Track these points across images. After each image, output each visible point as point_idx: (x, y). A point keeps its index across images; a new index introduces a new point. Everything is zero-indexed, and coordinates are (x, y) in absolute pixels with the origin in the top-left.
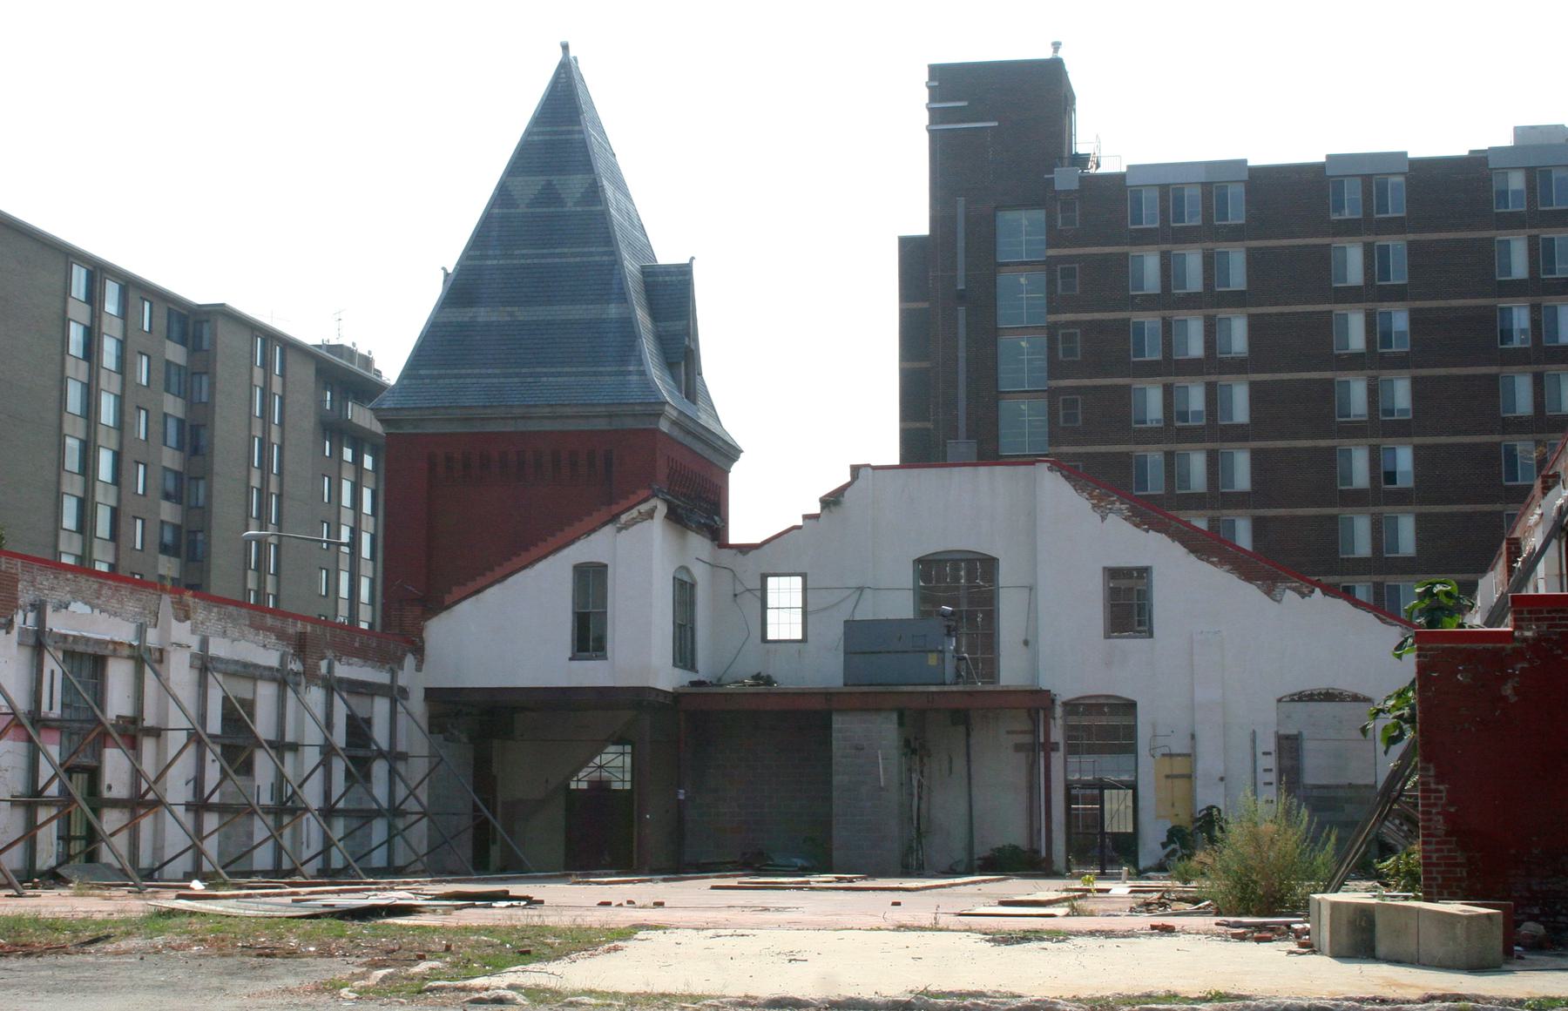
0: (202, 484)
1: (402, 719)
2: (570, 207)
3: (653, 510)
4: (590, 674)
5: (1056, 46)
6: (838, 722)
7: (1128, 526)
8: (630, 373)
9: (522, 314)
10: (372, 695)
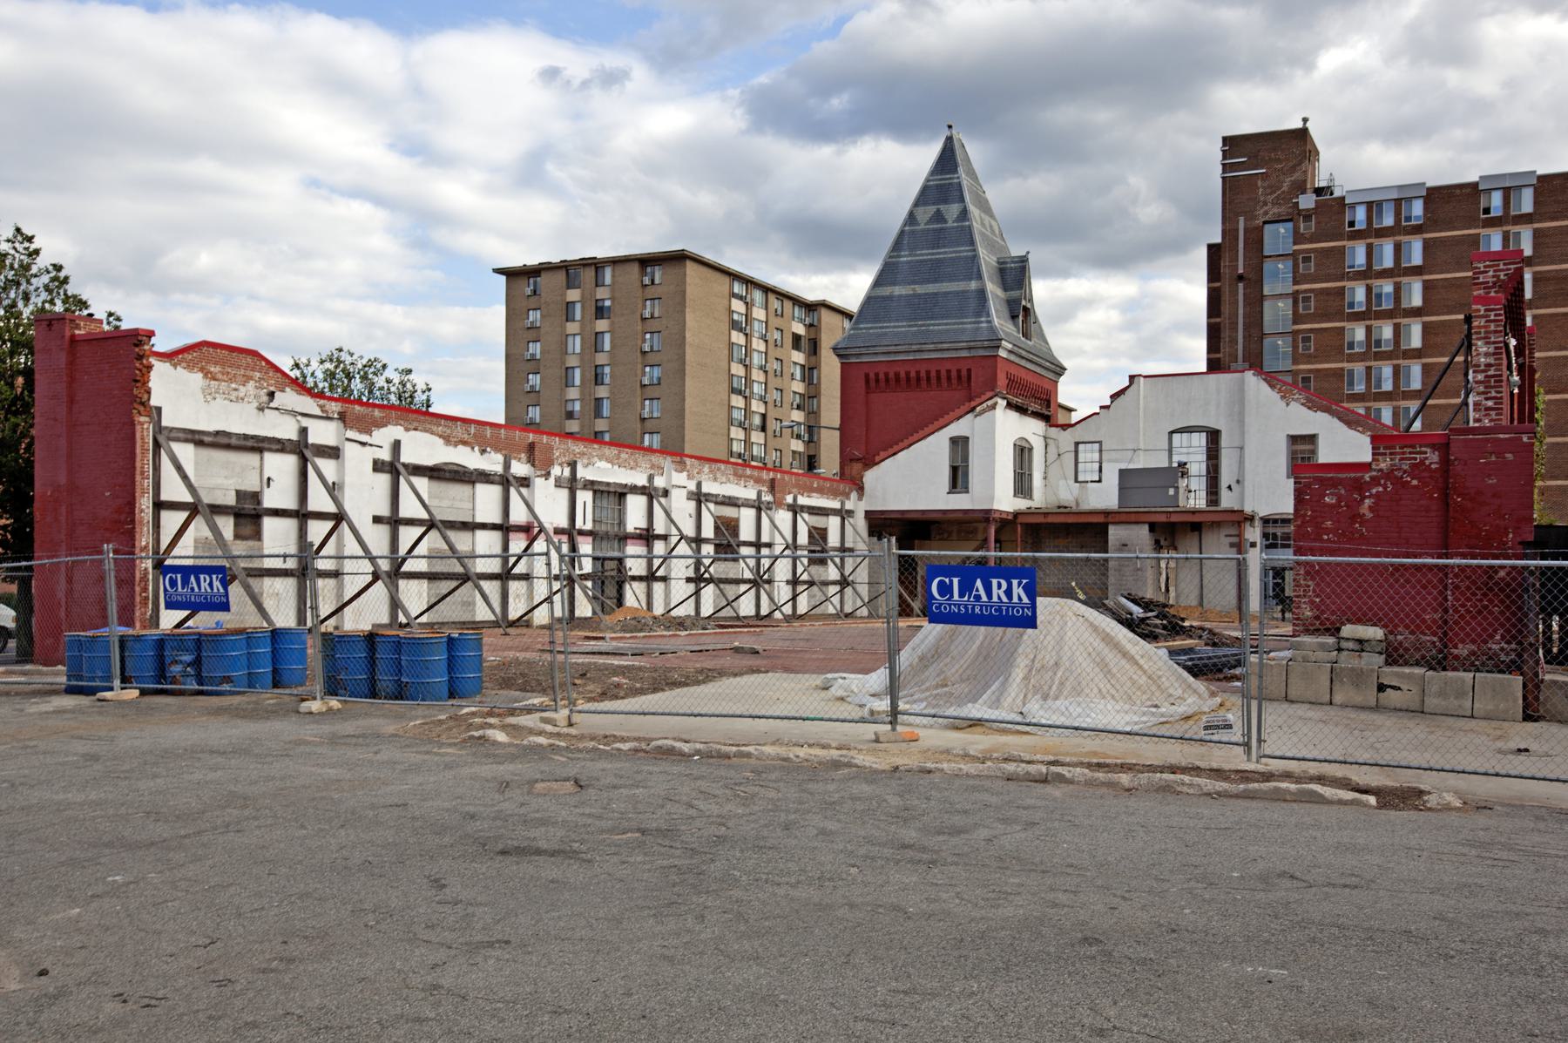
0: (815, 400)
1: (848, 528)
2: (950, 224)
3: (996, 404)
4: (959, 502)
5: (1305, 120)
7: (1304, 409)
8: (982, 322)
10: (828, 515)
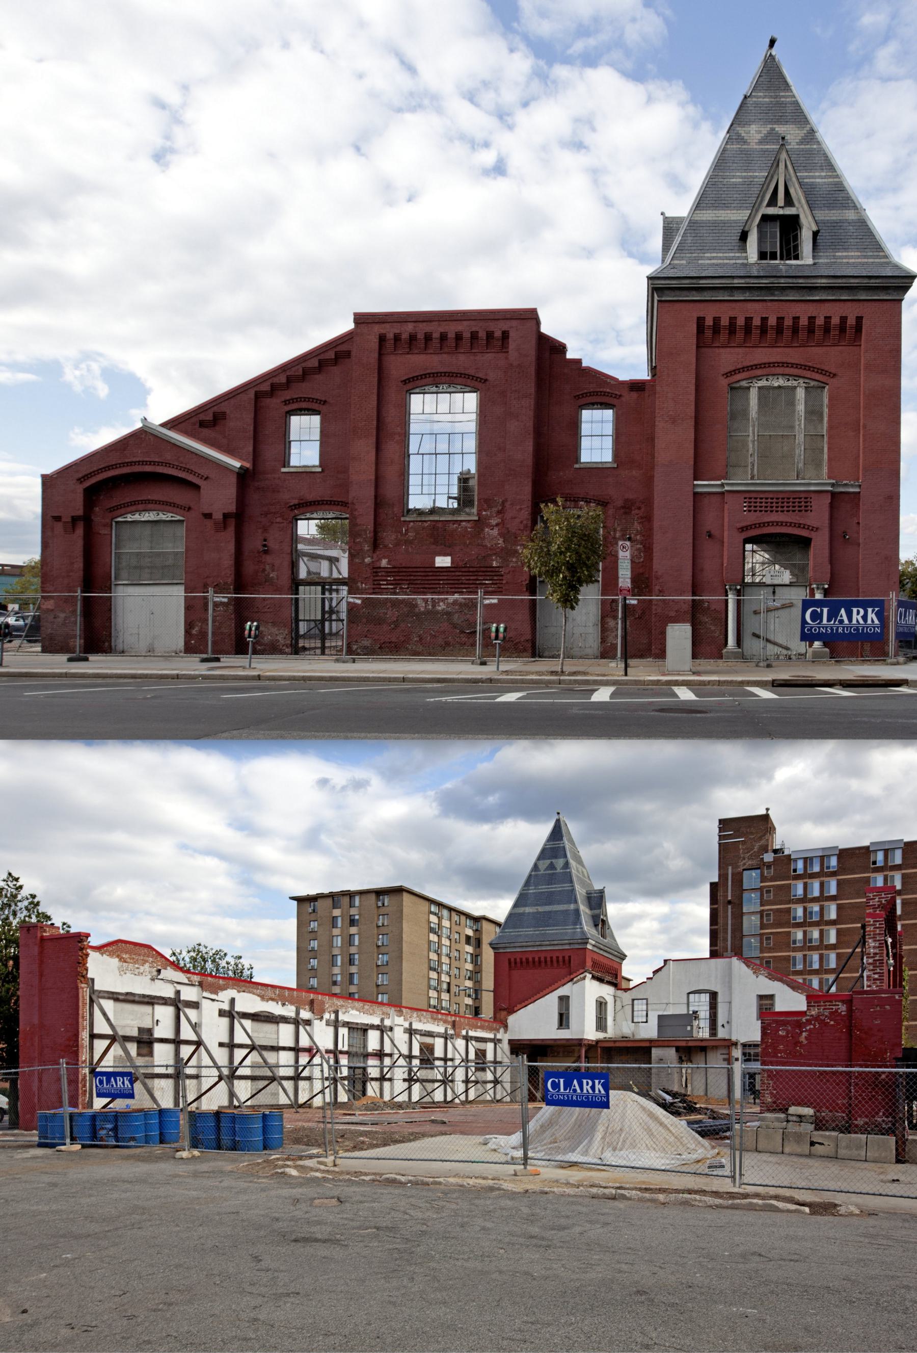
1: (498, 1049)
2: (559, 870)
3: (585, 976)
4: (564, 1034)
5: (767, 809)
6: (654, 1051)
7: (767, 980)
9: (541, 909)
